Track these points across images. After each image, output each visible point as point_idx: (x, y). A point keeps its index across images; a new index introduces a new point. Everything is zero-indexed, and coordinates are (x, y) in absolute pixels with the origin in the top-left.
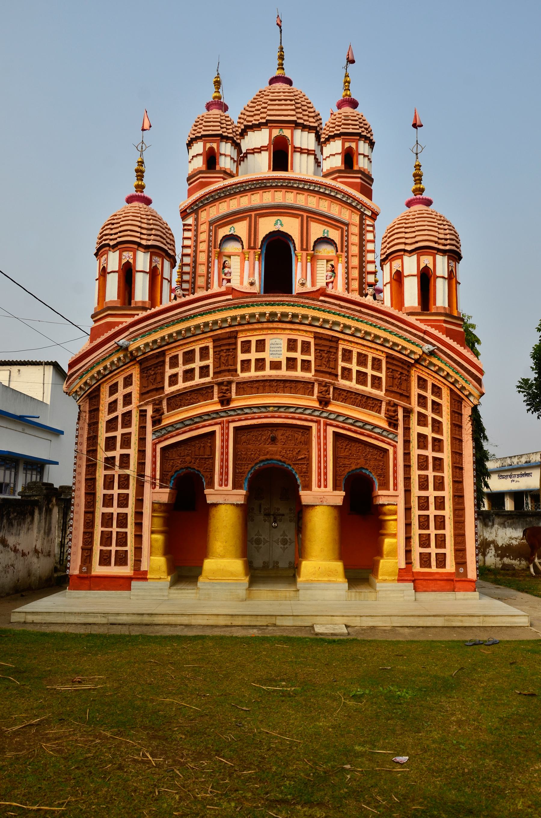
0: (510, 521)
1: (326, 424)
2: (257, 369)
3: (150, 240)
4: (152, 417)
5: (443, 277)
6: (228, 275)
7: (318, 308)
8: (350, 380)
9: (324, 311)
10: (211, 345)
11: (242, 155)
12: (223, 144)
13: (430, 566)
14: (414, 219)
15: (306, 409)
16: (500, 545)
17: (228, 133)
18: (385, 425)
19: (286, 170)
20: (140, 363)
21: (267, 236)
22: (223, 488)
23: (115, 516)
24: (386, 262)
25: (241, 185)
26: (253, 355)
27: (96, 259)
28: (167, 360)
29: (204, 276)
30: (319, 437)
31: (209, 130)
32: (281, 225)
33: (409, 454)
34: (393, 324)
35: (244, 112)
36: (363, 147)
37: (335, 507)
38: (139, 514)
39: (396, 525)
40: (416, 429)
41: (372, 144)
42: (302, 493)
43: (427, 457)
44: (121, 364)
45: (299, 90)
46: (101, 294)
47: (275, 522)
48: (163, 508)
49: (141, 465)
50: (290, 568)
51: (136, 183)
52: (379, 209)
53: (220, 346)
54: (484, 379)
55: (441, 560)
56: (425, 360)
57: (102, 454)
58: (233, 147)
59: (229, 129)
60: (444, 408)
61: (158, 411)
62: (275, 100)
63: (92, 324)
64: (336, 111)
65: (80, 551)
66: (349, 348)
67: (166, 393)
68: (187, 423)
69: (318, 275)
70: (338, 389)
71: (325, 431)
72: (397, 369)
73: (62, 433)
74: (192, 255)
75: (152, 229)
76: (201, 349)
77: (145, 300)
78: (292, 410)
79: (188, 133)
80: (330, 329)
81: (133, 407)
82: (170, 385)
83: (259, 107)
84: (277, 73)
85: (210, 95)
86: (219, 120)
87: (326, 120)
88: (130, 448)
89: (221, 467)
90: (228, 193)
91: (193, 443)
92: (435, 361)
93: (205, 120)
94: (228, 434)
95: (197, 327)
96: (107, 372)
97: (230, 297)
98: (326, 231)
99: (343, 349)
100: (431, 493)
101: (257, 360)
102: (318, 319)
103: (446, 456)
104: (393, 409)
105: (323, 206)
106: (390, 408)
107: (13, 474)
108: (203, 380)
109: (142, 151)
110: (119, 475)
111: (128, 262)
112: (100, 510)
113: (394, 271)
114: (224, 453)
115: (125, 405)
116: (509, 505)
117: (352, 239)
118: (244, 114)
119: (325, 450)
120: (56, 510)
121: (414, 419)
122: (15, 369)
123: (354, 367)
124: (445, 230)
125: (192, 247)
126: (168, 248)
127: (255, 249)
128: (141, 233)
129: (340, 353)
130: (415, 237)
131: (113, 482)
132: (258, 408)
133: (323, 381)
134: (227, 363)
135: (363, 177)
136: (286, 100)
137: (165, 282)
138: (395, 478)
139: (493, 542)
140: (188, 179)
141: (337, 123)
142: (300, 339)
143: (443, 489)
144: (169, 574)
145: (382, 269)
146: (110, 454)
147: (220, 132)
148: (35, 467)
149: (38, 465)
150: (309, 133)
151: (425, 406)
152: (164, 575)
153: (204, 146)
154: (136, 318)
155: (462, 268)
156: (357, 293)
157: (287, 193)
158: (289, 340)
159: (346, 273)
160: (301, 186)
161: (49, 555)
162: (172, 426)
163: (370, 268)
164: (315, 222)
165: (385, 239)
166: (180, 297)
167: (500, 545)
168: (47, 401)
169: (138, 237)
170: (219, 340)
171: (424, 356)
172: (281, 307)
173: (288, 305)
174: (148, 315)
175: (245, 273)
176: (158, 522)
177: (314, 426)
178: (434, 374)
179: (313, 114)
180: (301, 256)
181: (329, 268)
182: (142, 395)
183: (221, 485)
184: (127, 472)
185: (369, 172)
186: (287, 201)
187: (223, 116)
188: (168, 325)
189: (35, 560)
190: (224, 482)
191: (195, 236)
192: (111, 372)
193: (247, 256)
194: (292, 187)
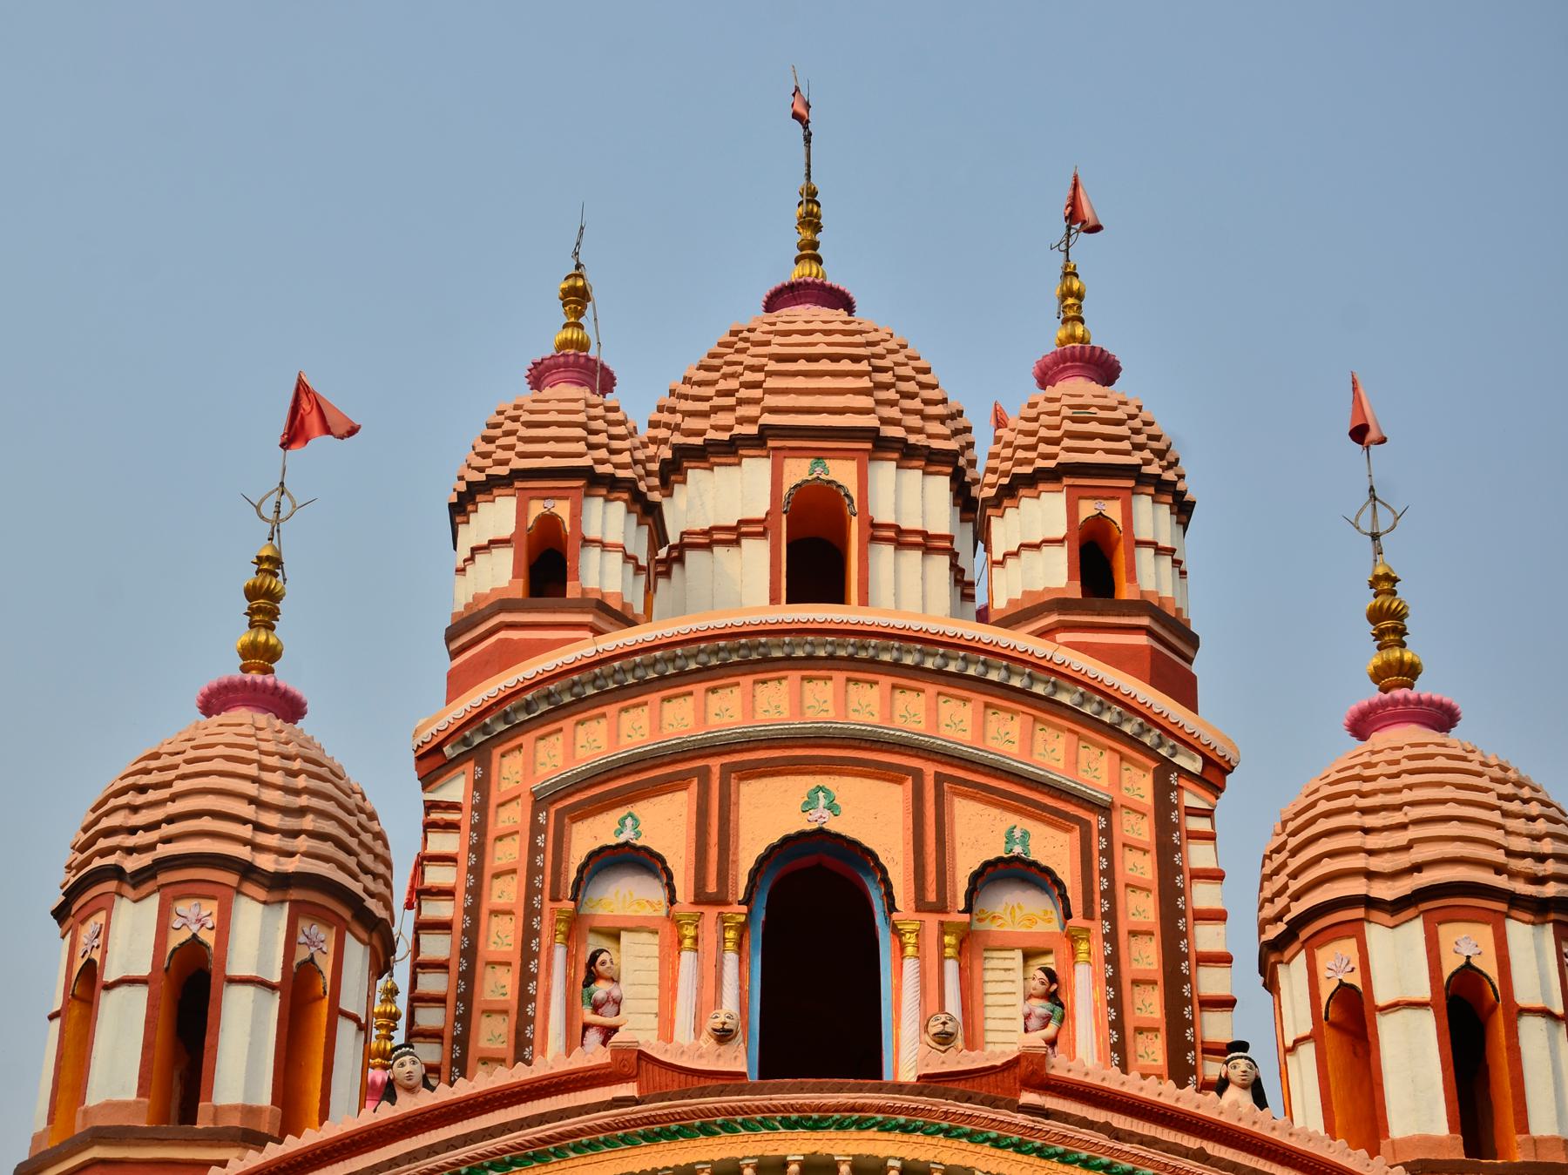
3: (291, 854)
5: (1546, 1013)
6: (610, 1008)
7: (1016, 1138)
11: (663, 553)
14: (1397, 775)
17: (616, 466)
21: (772, 851)
24: (1287, 954)
25: (667, 653)
27: (58, 930)
29: (505, 1012)
31: (540, 455)
32: (832, 807)
35: (673, 402)
36: (1151, 519)
41: (1183, 510)
46: (68, 1077)
51: (246, 636)
52: (1233, 747)
58: (634, 517)
59: (619, 452)
62: (793, 358)
69: (989, 1012)
74: (458, 927)
75: (302, 812)
77: (255, 1103)
79: (459, 467)
83: (733, 384)
84: (796, 273)
85: (547, 333)
86: (581, 418)
90: (612, 686)
93: (526, 417)
97: (628, 1090)
98: (1017, 833)
109: (277, 521)
111: (195, 943)
117: (1129, 865)
118: (672, 411)
124: (1532, 819)
125: (460, 893)
126: (366, 890)
127: (726, 903)
128: (259, 827)
130: (1408, 847)
135: (1157, 628)
137: (346, 1030)
140: (451, 635)
141: (1043, 433)
147: (586, 462)
150: (925, 473)
153: (522, 512)
157: (851, 686)
159: (1111, 1003)
160: (909, 660)
164: (973, 798)
165: (1278, 859)
166: (411, 1090)
169: (245, 842)
172: (853, 1133)
173: (883, 1127)
174: (268, 1165)
175: (685, 996)
179: (939, 410)
180: (918, 934)
181: (1035, 983)
185: (1179, 611)
186: (854, 717)
187: (595, 406)
191: (472, 849)
193: (689, 931)
194: (873, 665)
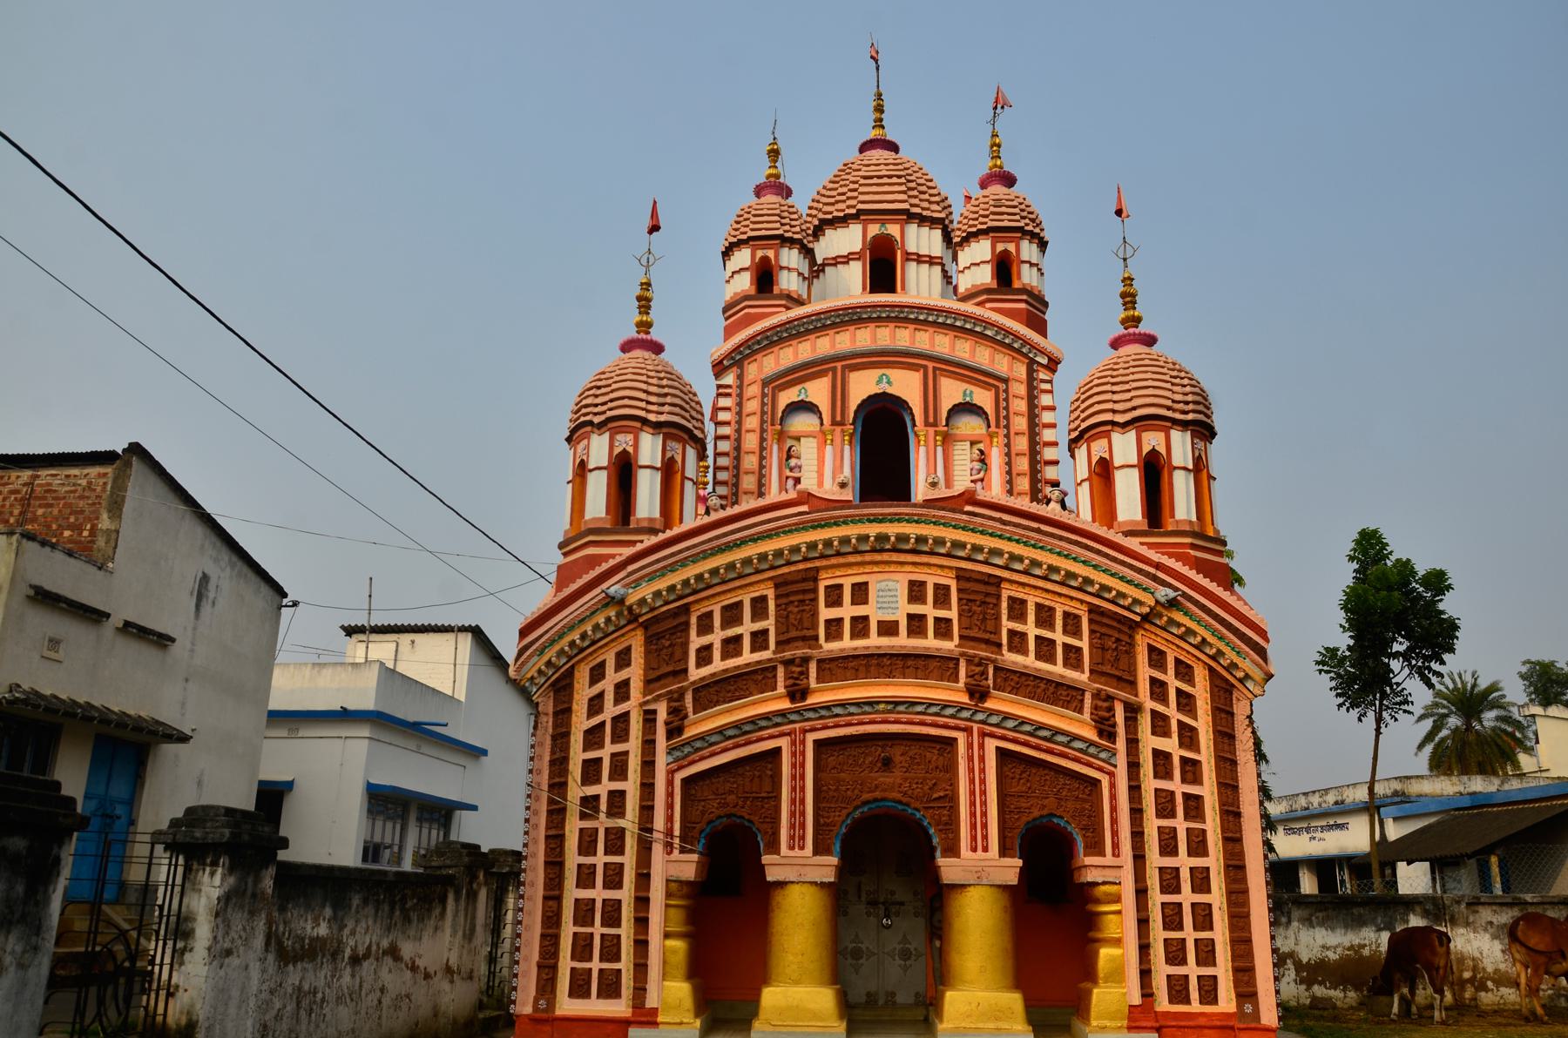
0: (1320, 915)
1: (983, 735)
2: (853, 636)
4: (667, 723)
8: (1025, 653)
9: (973, 531)
10: (770, 593)
12: (785, 252)
13: (1188, 1001)
15: (945, 707)
16: (1305, 961)
18: (1092, 735)
19: (892, 290)
20: (646, 626)
22: (797, 852)
23: (599, 905)
26: (847, 611)
28: (694, 620)
30: (970, 759)
32: (889, 383)
33: (1139, 787)
34: (1099, 552)
36: (1028, 250)
37: (1005, 888)
38: (642, 902)
39: (1119, 922)
40: (1149, 742)
41: (1043, 245)
42: (941, 861)
43: (1173, 793)
44: (612, 628)
45: (913, 160)
47: (887, 916)
48: (685, 889)
49: (647, 810)
50: (917, 1004)
51: (638, 318)
53: (787, 595)
54: (1271, 649)
55: (1209, 990)
56: (1161, 616)
57: (576, 791)
60: (1199, 703)
61: (677, 713)
63: (560, 559)
64: (976, 192)
65: (535, 970)
66: (1021, 596)
67: (692, 679)
68: (730, 733)
70: (1003, 669)
71: (982, 746)
72: (1110, 632)
73: (484, 752)
75: (666, 395)
76: (754, 600)
78: (920, 708)
80: (986, 562)
81: (632, 705)
82: (698, 665)
83: (844, 190)
84: (873, 134)
85: (761, 174)
87: (958, 210)
88: (626, 779)
89: (792, 814)
91: (740, 770)
92: (1178, 617)
94: (803, 753)
95: (747, 561)
96: (587, 643)
97: (804, 508)
99: (1010, 598)
100: (1184, 862)
101: (854, 619)
102: (963, 546)
103: (1208, 790)
104: (1105, 704)
105: (963, 350)
106: (1100, 703)
107: (398, 827)
108: (757, 656)
109: (648, 266)
110: (607, 829)
112: (572, 893)
113: (1095, 460)
114: (797, 790)
115: (617, 702)
116: (1308, 884)
119: (983, 781)
120: (483, 894)
121: (1145, 723)
122: (405, 639)
123: (1031, 630)
128: (648, 403)
129: (1004, 605)
131: (596, 841)
132: (858, 705)
133: (975, 656)
134: (800, 625)
136: (890, 177)
138: (1115, 834)
139: (1291, 955)
140: (725, 311)
142: (931, 581)
143: (1205, 854)
144: (697, 1016)
145: (1073, 456)
146: (591, 790)
148: (436, 816)
149: (440, 812)
151: (1163, 700)
152: (688, 1017)
153: (753, 256)
154: (639, 547)
155: (1217, 452)
156: (1027, 499)
158: (912, 583)
161: (471, 978)
162: (702, 738)
163: (1049, 454)
167: (1305, 961)
168: (461, 695)
170: (786, 583)
171: (1159, 608)
173: (908, 521)
175: (827, 466)
176: (677, 915)
177: (961, 737)
178: (1177, 641)
179: (937, 199)
182: (649, 683)
183: (792, 848)
184: (621, 823)
188: (695, 559)
189: (446, 986)
190: (797, 841)
192: (593, 643)
194: (906, 320)
